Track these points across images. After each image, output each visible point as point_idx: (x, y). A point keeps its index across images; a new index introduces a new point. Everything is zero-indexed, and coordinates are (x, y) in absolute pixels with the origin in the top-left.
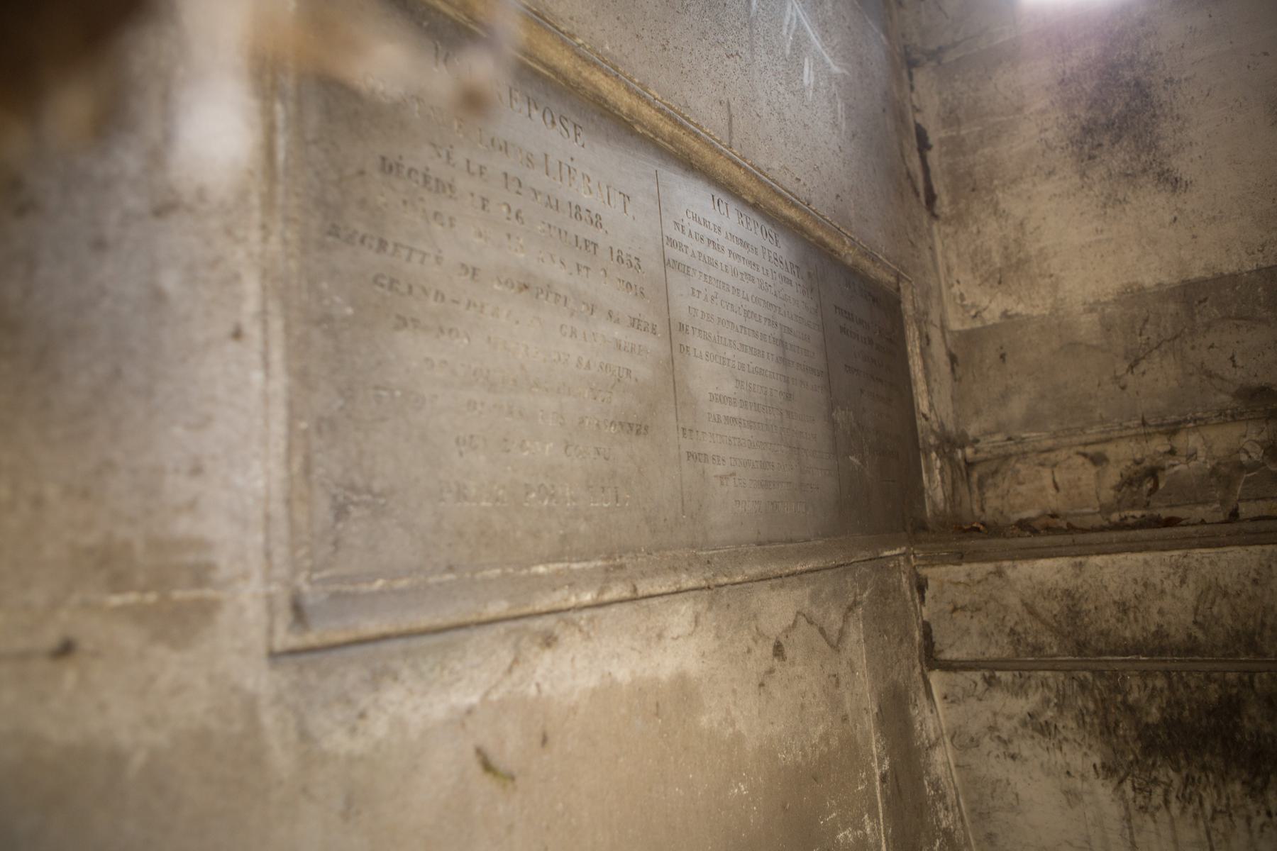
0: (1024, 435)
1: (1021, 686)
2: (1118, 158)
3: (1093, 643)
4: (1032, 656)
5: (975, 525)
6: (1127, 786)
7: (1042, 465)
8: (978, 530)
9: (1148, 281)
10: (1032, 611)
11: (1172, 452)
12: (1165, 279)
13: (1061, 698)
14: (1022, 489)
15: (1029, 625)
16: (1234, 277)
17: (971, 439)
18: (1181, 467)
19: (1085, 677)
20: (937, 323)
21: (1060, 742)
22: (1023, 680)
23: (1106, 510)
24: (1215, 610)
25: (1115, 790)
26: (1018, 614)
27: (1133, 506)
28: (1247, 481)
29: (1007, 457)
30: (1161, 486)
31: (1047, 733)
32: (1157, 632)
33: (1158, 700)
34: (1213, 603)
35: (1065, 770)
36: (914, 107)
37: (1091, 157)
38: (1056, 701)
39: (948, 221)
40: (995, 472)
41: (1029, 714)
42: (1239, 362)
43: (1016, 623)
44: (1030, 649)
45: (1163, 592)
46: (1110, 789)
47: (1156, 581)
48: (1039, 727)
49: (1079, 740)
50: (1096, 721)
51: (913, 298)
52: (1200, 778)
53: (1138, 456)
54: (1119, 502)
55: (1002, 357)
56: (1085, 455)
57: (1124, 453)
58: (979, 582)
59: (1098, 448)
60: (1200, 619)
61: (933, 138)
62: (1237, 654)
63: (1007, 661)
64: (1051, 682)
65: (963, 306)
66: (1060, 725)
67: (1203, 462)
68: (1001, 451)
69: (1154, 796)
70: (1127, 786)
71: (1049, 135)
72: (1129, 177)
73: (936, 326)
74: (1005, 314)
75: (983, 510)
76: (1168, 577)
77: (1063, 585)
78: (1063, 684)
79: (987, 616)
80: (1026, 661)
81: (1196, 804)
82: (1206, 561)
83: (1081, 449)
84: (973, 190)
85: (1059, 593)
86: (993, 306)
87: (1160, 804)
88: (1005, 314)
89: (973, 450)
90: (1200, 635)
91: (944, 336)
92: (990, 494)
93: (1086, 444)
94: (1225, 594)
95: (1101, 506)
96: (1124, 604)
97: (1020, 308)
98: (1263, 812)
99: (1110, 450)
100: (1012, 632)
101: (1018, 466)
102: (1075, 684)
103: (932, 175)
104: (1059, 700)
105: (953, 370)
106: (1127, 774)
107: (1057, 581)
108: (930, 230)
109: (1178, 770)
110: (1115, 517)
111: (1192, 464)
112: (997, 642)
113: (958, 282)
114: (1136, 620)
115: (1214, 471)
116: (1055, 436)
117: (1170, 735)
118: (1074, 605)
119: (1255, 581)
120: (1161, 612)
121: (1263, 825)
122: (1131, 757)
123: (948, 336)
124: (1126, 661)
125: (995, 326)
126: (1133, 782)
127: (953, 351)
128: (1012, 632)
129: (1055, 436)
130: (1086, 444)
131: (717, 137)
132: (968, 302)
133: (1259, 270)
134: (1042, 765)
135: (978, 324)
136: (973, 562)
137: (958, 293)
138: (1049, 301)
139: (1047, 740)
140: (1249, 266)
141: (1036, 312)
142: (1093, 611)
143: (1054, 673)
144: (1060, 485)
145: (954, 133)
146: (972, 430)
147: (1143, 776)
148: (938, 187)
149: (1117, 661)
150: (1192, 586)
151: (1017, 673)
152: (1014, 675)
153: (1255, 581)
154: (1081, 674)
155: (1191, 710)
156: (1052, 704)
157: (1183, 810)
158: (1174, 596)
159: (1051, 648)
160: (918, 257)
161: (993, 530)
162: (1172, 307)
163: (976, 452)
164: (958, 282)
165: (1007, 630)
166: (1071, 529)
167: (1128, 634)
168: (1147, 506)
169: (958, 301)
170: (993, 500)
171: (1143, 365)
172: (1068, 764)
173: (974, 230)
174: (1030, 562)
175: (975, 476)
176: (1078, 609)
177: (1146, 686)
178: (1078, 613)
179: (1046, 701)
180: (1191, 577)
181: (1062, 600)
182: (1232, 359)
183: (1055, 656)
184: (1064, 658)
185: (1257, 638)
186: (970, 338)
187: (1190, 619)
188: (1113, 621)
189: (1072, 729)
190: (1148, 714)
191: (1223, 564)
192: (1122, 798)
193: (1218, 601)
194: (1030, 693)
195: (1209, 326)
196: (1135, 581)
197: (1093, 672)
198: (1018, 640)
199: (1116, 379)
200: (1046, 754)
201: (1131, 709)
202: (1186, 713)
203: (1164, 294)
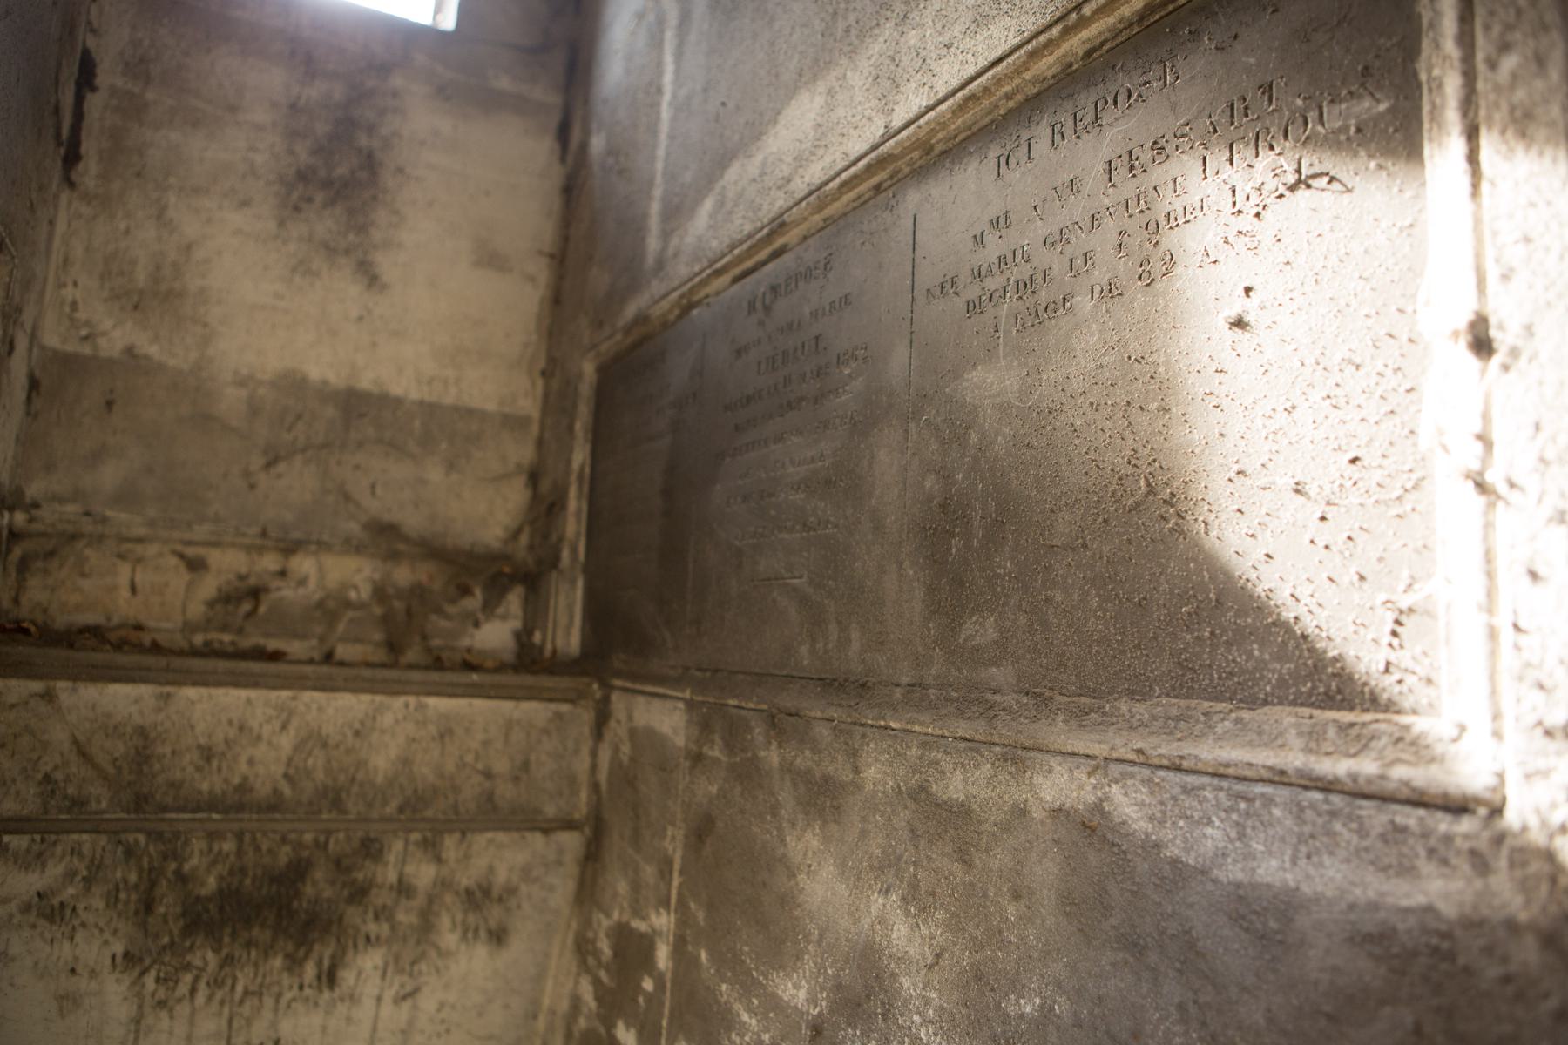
0: (109, 513)
1: (40, 855)
2: (326, 224)
3: (158, 797)
4: (68, 813)
5: (25, 625)
6: (149, 981)
7: (121, 557)
8: (26, 632)
9: (314, 373)
10: (83, 753)
11: (283, 574)
12: (332, 377)
13: (94, 869)
14: (85, 584)
15: (74, 769)
16: (399, 401)
17: (28, 500)
18: (287, 593)
19: (136, 841)
20: (28, 327)
21: (74, 928)
22: (44, 846)
23: (189, 628)
24: (310, 762)
25: (133, 984)
26: (62, 755)
27: (224, 628)
28: (352, 621)
29: (74, 537)
30: (262, 609)
31: (58, 919)
32: (240, 785)
33: (219, 867)
34: (310, 754)
35: (69, 968)
36: (89, 23)
37: (297, 209)
38: (85, 873)
39: (87, 198)
40: (51, 554)
41: (39, 894)
42: (379, 491)
43: (56, 768)
44: (67, 803)
45: (259, 738)
46: (123, 988)
47: (255, 724)
48: (48, 911)
49: (101, 924)
50: (134, 897)
51: (10, 281)
52: (240, 957)
53: (244, 570)
54: (209, 621)
55: (109, 404)
56: (181, 556)
57: (228, 563)
58: (13, 706)
59: (201, 551)
60: (292, 771)
61: (103, 79)
62: (320, 812)
63: (28, 820)
64: (86, 849)
65: (72, 319)
66: (81, 906)
67: (312, 591)
68: (70, 528)
69: (180, 985)
70: (149, 981)
71: (259, 159)
72: (330, 250)
73: (25, 331)
74: (129, 351)
75: (16, 601)
76: (269, 720)
77: (137, 720)
78: (103, 850)
79: (13, 755)
80: (58, 820)
81: (227, 989)
82: (314, 706)
83: (179, 548)
84: (138, 175)
85: (129, 730)
86: (117, 334)
87: (184, 995)
88: (129, 351)
89: (27, 516)
90: (287, 791)
91: (30, 350)
92: (34, 582)
93: (189, 543)
94: (325, 745)
95: (186, 623)
96: (210, 749)
97: (153, 350)
98: (296, 987)
99: (215, 557)
100: (47, 778)
101: (88, 552)
102: (120, 849)
103: (85, 124)
104: (90, 872)
105: (29, 399)
106: (154, 962)
107: (130, 715)
108: (56, 197)
109: (217, 951)
110: (198, 639)
111: (301, 591)
112: (18, 793)
113: (75, 284)
114: (219, 769)
115: (320, 604)
116: (151, 523)
117: (221, 909)
118: (145, 748)
119: (357, 734)
120: (251, 762)
121: (294, 999)
122: (166, 940)
123: (35, 350)
124: (194, 820)
125: (110, 361)
126: (159, 971)
127: (37, 373)
128: (47, 778)
129: (151, 523)
130: (189, 543)
131: (697, 269)
132: (82, 315)
133: (421, 403)
134: (36, 964)
135: (87, 350)
136: (12, 676)
137: (70, 298)
138: (193, 355)
139: (55, 928)
140: (414, 395)
141: (172, 362)
142: (169, 755)
143: (94, 836)
144: (139, 586)
145: (137, 90)
146: (33, 490)
147: (173, 963)
148: (88, 146)
149: (184, 820)
150: (292, 732)
151: (38, 837)
152: (33, 840)
153: (357, 734)
154: (131, 838)
155: (254, 880)
156: (78, 878)
157: (210, 998)
158: (270, 743)
159: (99, 802)
160: (33, 228)
161: (71, 638)
162: (330, 412)
163: (31, 520)
164: (75, 284)
165: (39, 776)
166: (156, 648)
167: (205, 786)
168: (240, 631)
169: (67, 309)
170: (36, 592)
171: (281, 467)
172: (76, 959)
173: (122, 226)
174: (100, 686)
175: (17, 552)
176: (148, 752)
177: (210, 850)
178: (148, 758)
179: (70, 875)
180: (295, 722)
181: (131, 739)
182: (373, 487)
183: (103, 812)
184: (113, 816)
185: (344, 795)
186: (68, 364)
187: (281, 770)
188: (190, 769)
189: (97, 910)
190: (203, 884)
191: (330, 711)
192: (139, 995)
193: (316, 752)
194: (50, 863)
195: (360, 444)
196: (230, 722)
197: (149, 834)
198: (53, 791)
199: (247, 474)
200: (47, 949)
201: (182, 878)
202: (248, 882)
203: (326, 394)
